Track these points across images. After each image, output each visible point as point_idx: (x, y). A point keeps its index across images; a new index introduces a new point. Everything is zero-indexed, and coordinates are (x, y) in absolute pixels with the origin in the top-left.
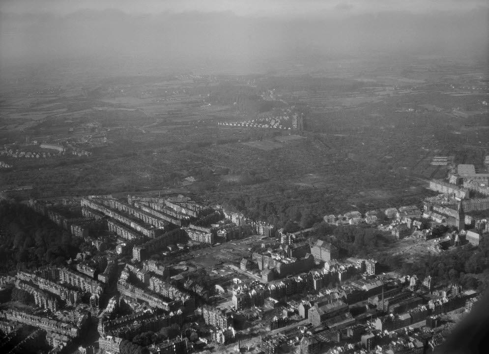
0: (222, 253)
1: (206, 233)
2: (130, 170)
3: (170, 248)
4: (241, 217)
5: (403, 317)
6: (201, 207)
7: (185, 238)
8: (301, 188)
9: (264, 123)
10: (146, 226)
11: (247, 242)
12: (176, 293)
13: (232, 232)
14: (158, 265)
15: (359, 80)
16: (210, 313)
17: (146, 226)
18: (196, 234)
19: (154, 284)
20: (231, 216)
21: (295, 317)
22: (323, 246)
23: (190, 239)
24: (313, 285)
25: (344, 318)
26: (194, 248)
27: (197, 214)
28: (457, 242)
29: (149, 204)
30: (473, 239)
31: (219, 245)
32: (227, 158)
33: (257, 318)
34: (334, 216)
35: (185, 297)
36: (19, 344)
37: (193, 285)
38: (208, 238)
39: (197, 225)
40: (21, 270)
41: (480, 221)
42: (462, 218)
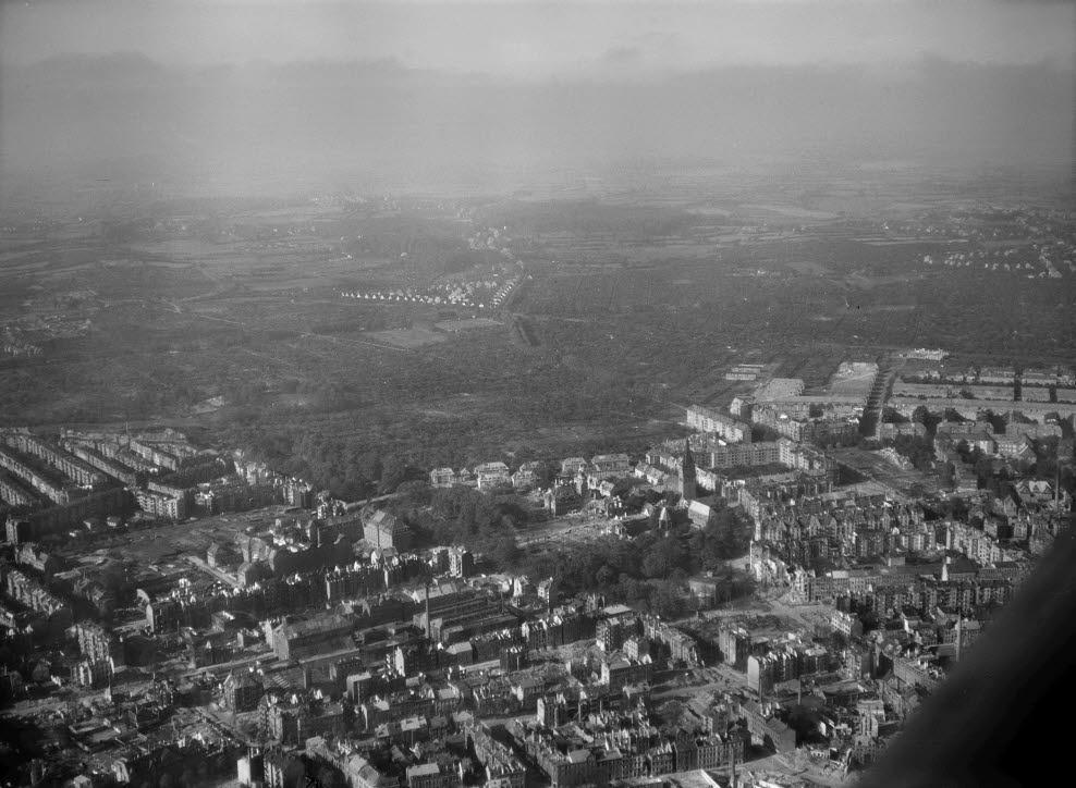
0: (195, 533)
1: (170, 497)
2: (102, 383)
3: (89, 525)
4: (260, 470)
5: (454, 650)
6: (195, 451)
7: (131, 505)
8: (426, 420)
9: (435, 293)
10: (57, 479)
11: (251, 517)
12: (43, 599)
13: (226, 497)
14: (37, 552)
15: (692, 211)
16: (87, 632)
17: (57, 479)
18: (152, 499)
19: (13, 583)
20: (245, 470)
21: (254, 648)
22: (383, 522)
23: (138, 508)
24: (326, 593)
25: (340, 646)
26: (141, 525)
27: (177, 465)
28: (663, 522)
29: (96, 446)
30: (699, 516)
31: (192, 522)
32: (316, 361)
33: (183, 646)
34: (450, 470)
35: (54, 606)
36: (449, 677)
37: (90, 588)
38: (171, 508)
39: (160, 484)
40: (608, 537)
41: (732, 484)
42: (690, 475)
